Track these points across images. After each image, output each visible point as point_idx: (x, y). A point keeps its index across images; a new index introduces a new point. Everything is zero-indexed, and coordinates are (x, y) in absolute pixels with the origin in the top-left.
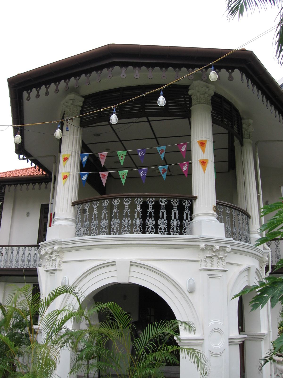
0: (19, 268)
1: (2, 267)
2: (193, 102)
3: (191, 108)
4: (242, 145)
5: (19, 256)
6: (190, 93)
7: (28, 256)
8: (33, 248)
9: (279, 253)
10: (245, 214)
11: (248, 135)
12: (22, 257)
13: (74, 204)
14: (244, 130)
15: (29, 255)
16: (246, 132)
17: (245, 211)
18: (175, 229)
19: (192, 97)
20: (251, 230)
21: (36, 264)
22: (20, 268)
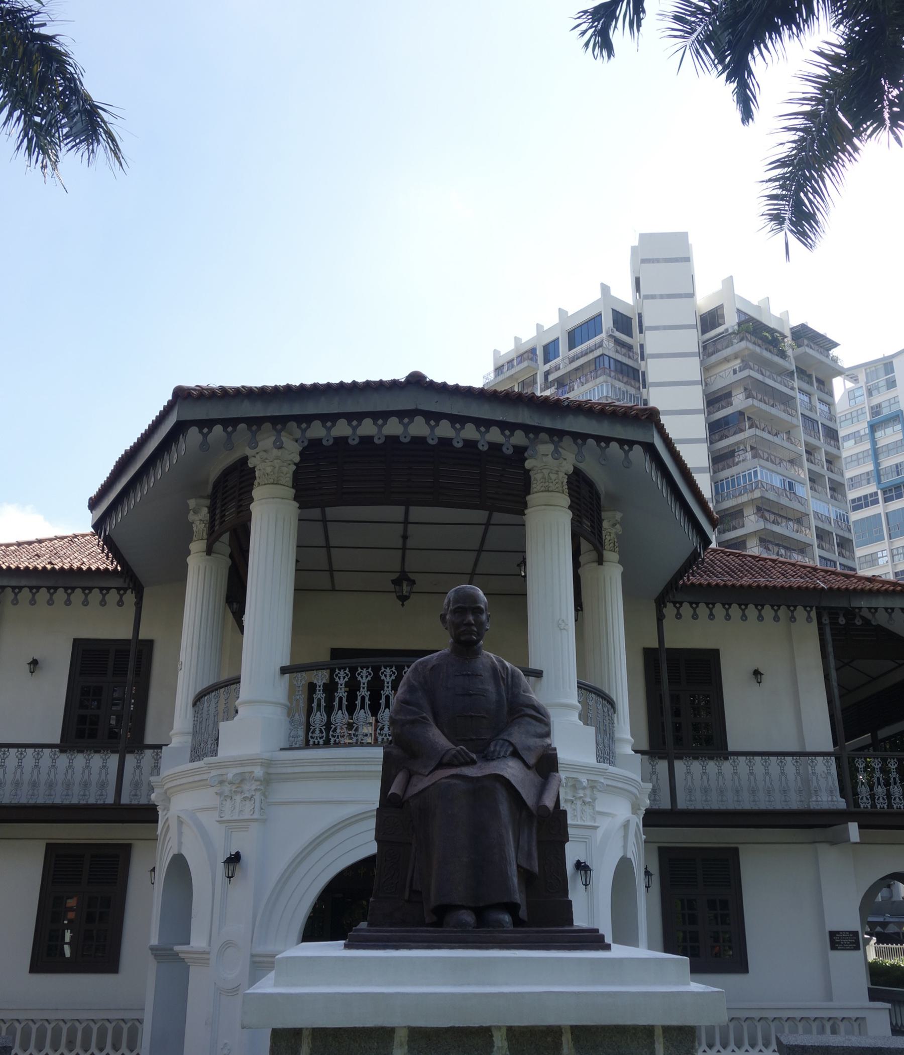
0: (90, 802)
1: (6, 800)
2: (535, 486)
3: (528, 498)
4: (600, 561)
5: (39, 771)
6: (528, 464)
7: (50, 771)
8: (47, 751)
9: (72, 777)
10: (608, 702)
11: (612, 545)
12: (717, 780)
13: (284, 670)
14: (604, 533)
15: (70, 771)
16: (608, 538)
17: (605, 694)
18: (317, 731)
19: (531, 473)
20: (617, 735)
21: (53, 793)
22: (77, 802)
